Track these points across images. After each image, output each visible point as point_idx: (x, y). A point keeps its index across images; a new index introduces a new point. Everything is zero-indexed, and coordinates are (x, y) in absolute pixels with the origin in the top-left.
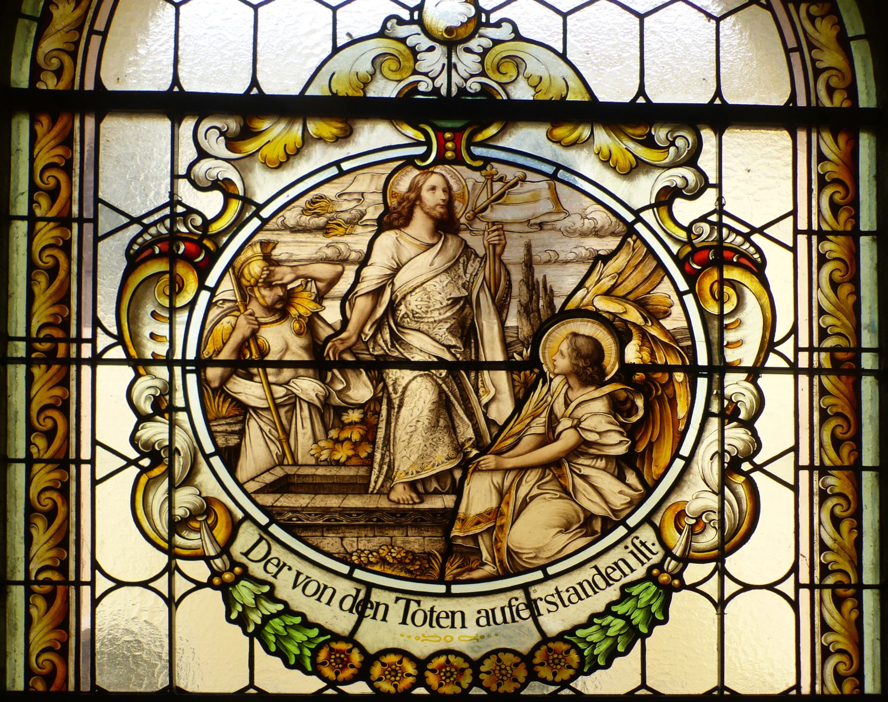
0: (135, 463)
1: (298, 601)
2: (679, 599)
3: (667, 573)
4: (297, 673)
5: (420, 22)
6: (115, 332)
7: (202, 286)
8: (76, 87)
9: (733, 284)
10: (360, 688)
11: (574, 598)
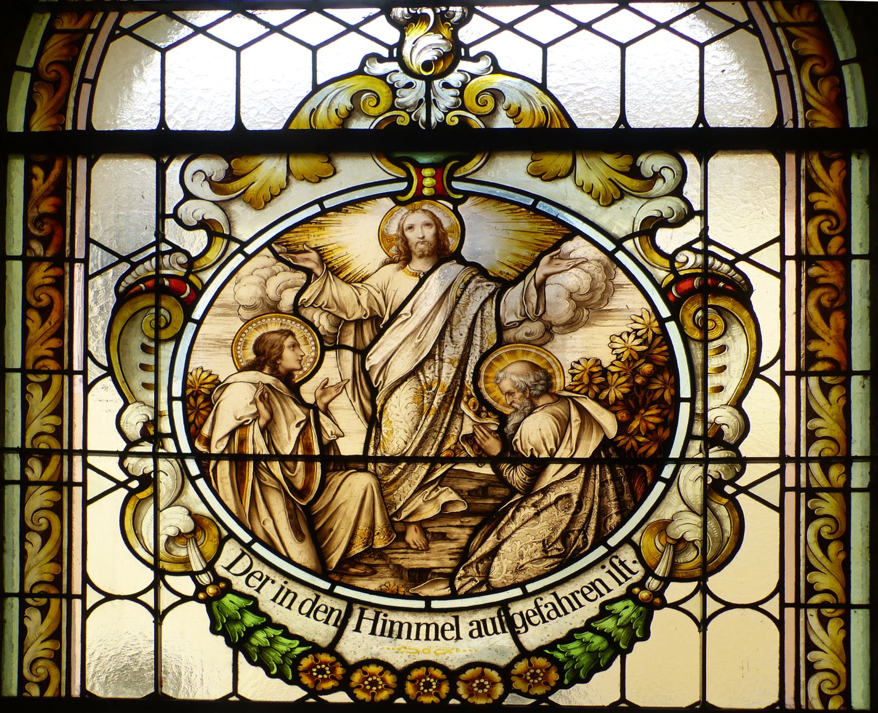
1: (278, 614)
2: (660, 617)
4: (278, 682)
5: (400, 59)
6: (106, 364)
8: (63, 694)
9: (720, 310)
10: (341, 697)
11: (553, 614)
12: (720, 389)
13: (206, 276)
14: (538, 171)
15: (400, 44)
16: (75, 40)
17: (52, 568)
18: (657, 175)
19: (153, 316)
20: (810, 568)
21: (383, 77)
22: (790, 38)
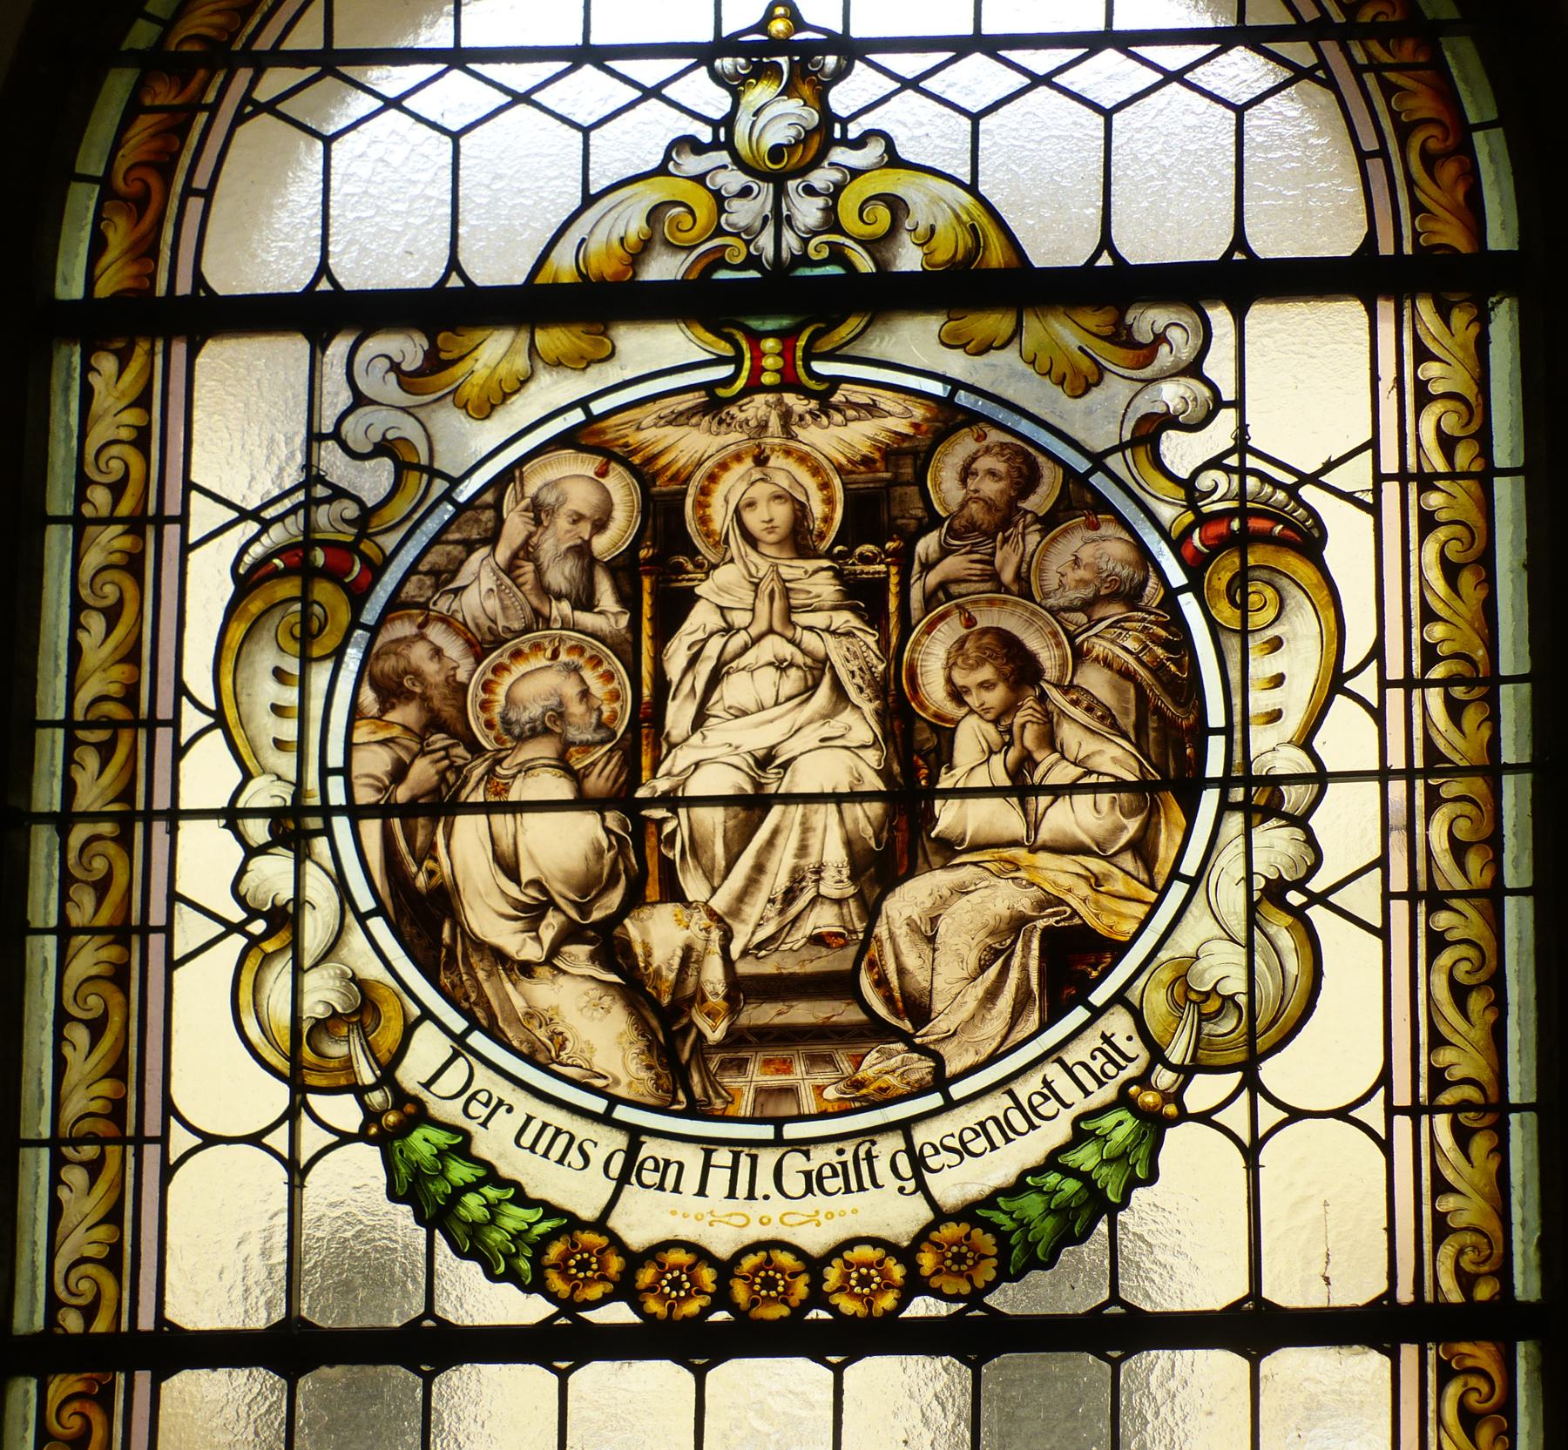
0: (239, 928)
3: (1156, 1090)
4: (508, 1288)
5: (729, 145)
6: (212, 706)
7: (355, 624)
8: (124, 1327)
12: (1275, 716)
13: (389, 542)
14: (957, 337)
15: (729, 121)
16: (177, 125)
17: (120, 672)
18: (1160, 338)
19: (298, 618)
20: (1437, 1041)
21: (700, 179)
22: (1388, 89)
